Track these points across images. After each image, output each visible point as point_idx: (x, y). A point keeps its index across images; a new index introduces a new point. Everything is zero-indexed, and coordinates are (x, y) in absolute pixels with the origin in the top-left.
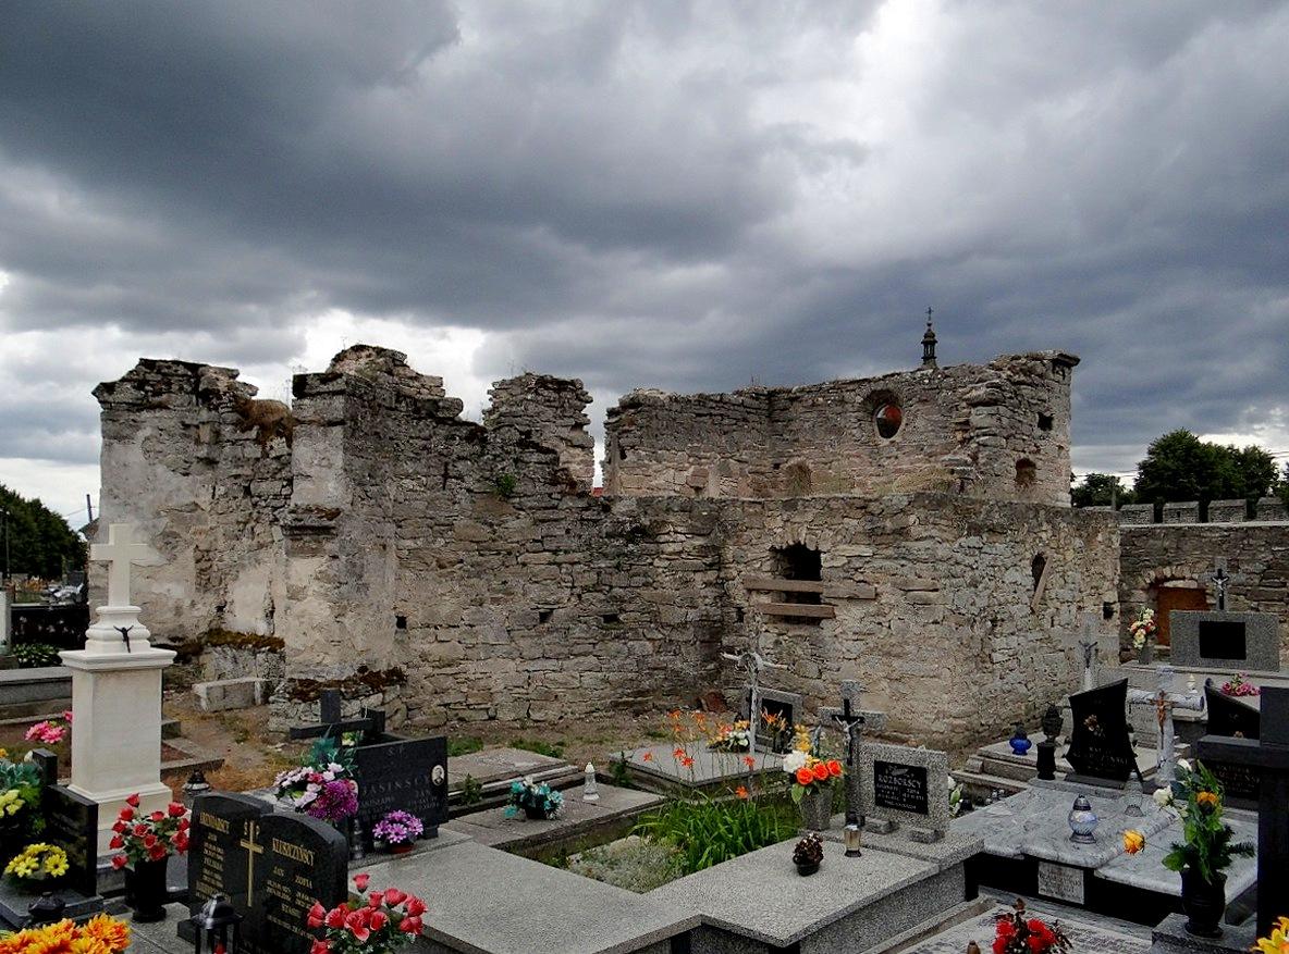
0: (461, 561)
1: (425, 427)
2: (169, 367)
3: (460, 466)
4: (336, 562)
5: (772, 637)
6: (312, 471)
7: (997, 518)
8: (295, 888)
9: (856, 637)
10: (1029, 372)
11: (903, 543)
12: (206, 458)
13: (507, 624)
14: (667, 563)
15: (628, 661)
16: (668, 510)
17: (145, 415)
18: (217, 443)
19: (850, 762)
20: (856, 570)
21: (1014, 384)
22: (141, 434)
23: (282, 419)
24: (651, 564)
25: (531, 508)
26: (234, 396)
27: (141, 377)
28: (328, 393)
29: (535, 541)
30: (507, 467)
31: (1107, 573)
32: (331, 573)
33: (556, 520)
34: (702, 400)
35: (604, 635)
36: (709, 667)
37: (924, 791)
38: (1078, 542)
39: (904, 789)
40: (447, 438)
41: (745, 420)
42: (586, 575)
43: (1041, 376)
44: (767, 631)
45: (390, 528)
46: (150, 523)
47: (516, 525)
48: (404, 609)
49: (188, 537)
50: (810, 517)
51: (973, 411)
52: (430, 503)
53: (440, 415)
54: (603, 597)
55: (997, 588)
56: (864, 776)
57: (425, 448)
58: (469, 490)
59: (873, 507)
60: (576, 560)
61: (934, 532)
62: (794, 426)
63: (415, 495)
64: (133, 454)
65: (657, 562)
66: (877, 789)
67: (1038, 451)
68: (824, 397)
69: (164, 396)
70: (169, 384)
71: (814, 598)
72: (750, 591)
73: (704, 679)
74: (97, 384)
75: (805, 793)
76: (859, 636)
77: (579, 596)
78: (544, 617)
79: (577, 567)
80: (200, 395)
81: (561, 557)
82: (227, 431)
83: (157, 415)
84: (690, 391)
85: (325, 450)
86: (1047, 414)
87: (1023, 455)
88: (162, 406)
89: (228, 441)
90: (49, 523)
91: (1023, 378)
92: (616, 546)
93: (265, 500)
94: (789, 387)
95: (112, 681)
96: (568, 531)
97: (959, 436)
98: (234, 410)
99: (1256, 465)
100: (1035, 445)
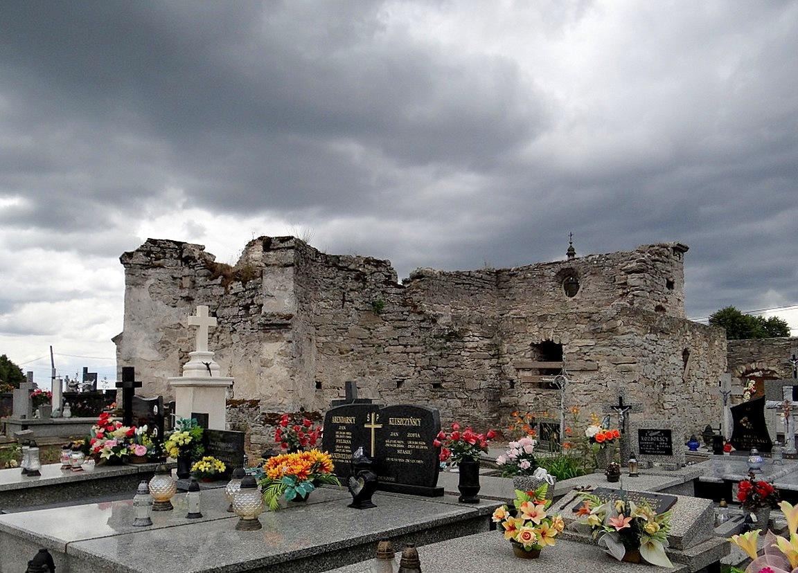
0: (352, 350)
1: (332, 272)
2: (165, 244)
3: (352, 294)
4: (290, 345)
5: (532, 396)
6: (275, 293)
7: (664, 325)
8: (406, 440)
9: (586, 393)
10: (660, 254)
11: (614, 337)
12: (187, 297)
13: (378, 387)
14: (469, 353)
15: (447, 411)
16: (469, 323)
17: (151, 271)
18: (194, 288)
19: (623, 431)
20: (585, 354)
21: (653, 261)
22: (149, 283)
23: (239, 271)
24: (460, 354)
25: (391, 320)
26: (205, 260)
27: (149, 249)
28: (284, 248)
29: (394, 339)
30: (377, 296)
31: (720, 364)
32: (288, 351)
33: (405, 327)
34: (458, 274)
35: (434, 395)
36: (493, 416)
37: (670, 442)
38: (705, 344)
39: (658, 443)
40: (343, 278)
41: (483, 287)
42: (423, 359)
43: (667, 257)
44: (529, 393)
45: (313, 330)
46: (153, 335)
47: (384, 330)
48: (321, 378)
49: (175, 343)
50: (555, 324)
51: (629, 276)
52: (335, 316)
53: (340, 265)
54: (433, 373)
55: (665, 366)
56: (633, 438)
57: (332, 283)
58: (357, 309)
59: (595, 317)
60: (417, 351)
61: (633, 329)
62: (513, 291)
63: (326, 311)
64: (143, 294)
65: (463, 353)
66: (640, 445)
67: (667, 301)
68: (531, 273)
69: (162, 260)
70: (165, 253)
71: (557, 372)
72: (518, 370)
73: (491, 422)
74: (123, 252)
75: (601, 448)
76: (587, 392)
77: (419, 372)
78: (399, 384)
79: (418, 355)
80: (183, 260)
81: (409, 349)
82: (200, 281)
83: (158, 271)
84: (452, 270)
85: (283, 281)
86: (671, 280)
87: (658, 303)
88: (160, 266)
89: (201, 286)
90: (12, 370)
91: (657, 257)
92: (440, 343)
93: (227, 319)
94: (509, 268)
95: (202, 391)
96: (412, 334)
97: (620, 292)
98: (205, 267)
99: (778, 328)
100: (665, 298)
